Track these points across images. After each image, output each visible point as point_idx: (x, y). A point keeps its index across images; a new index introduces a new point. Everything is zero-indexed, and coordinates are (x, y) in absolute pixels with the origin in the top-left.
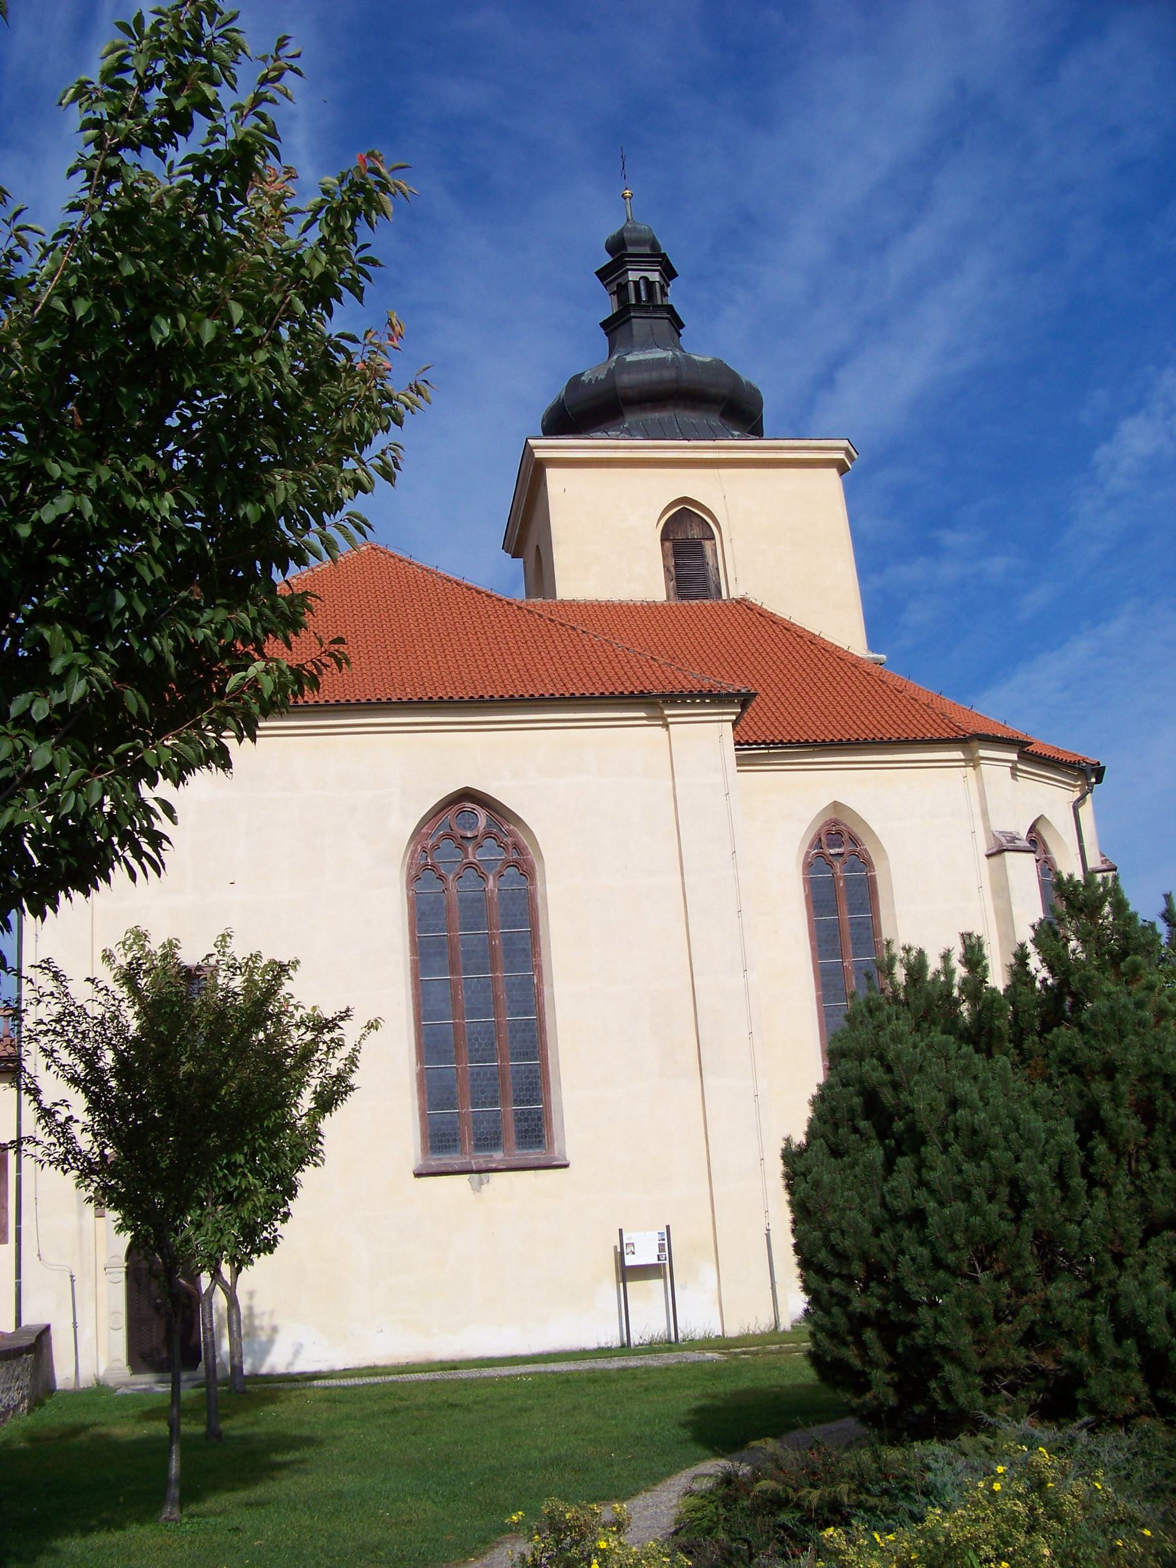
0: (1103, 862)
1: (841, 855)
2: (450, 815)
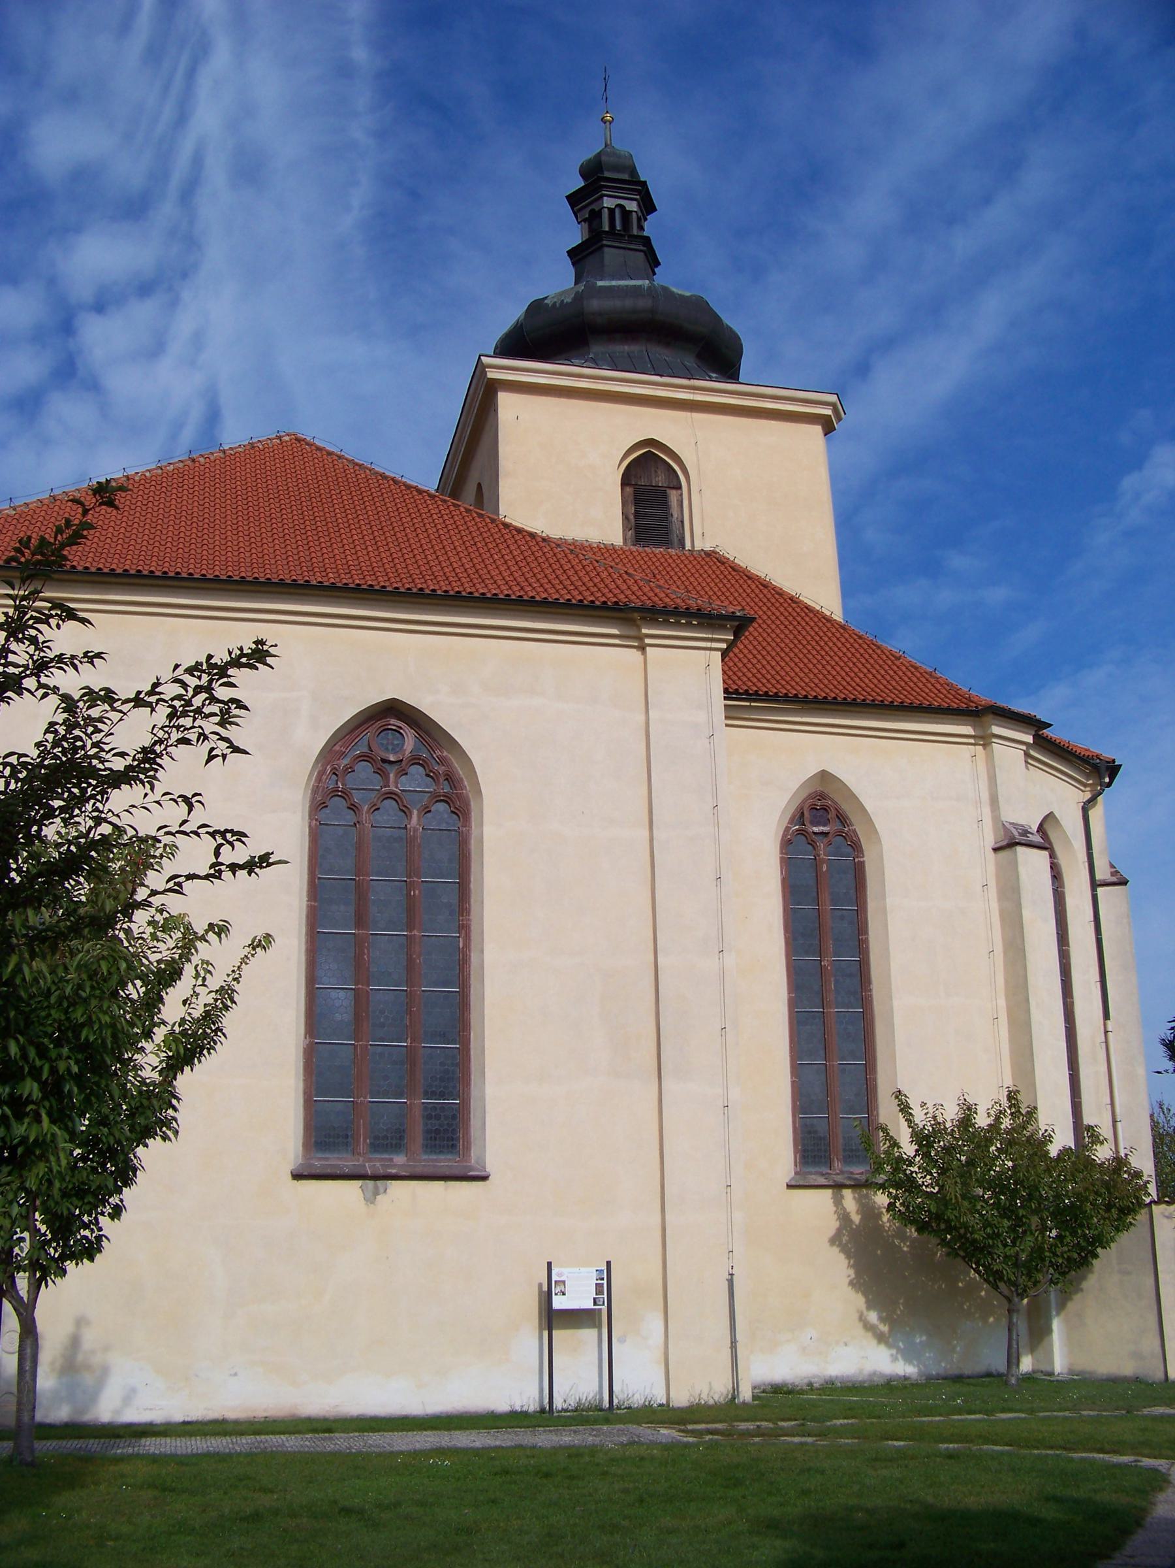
0: (1113, 874)
2: (369, 734)
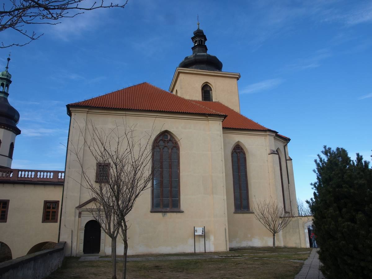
1: (239, 152)
